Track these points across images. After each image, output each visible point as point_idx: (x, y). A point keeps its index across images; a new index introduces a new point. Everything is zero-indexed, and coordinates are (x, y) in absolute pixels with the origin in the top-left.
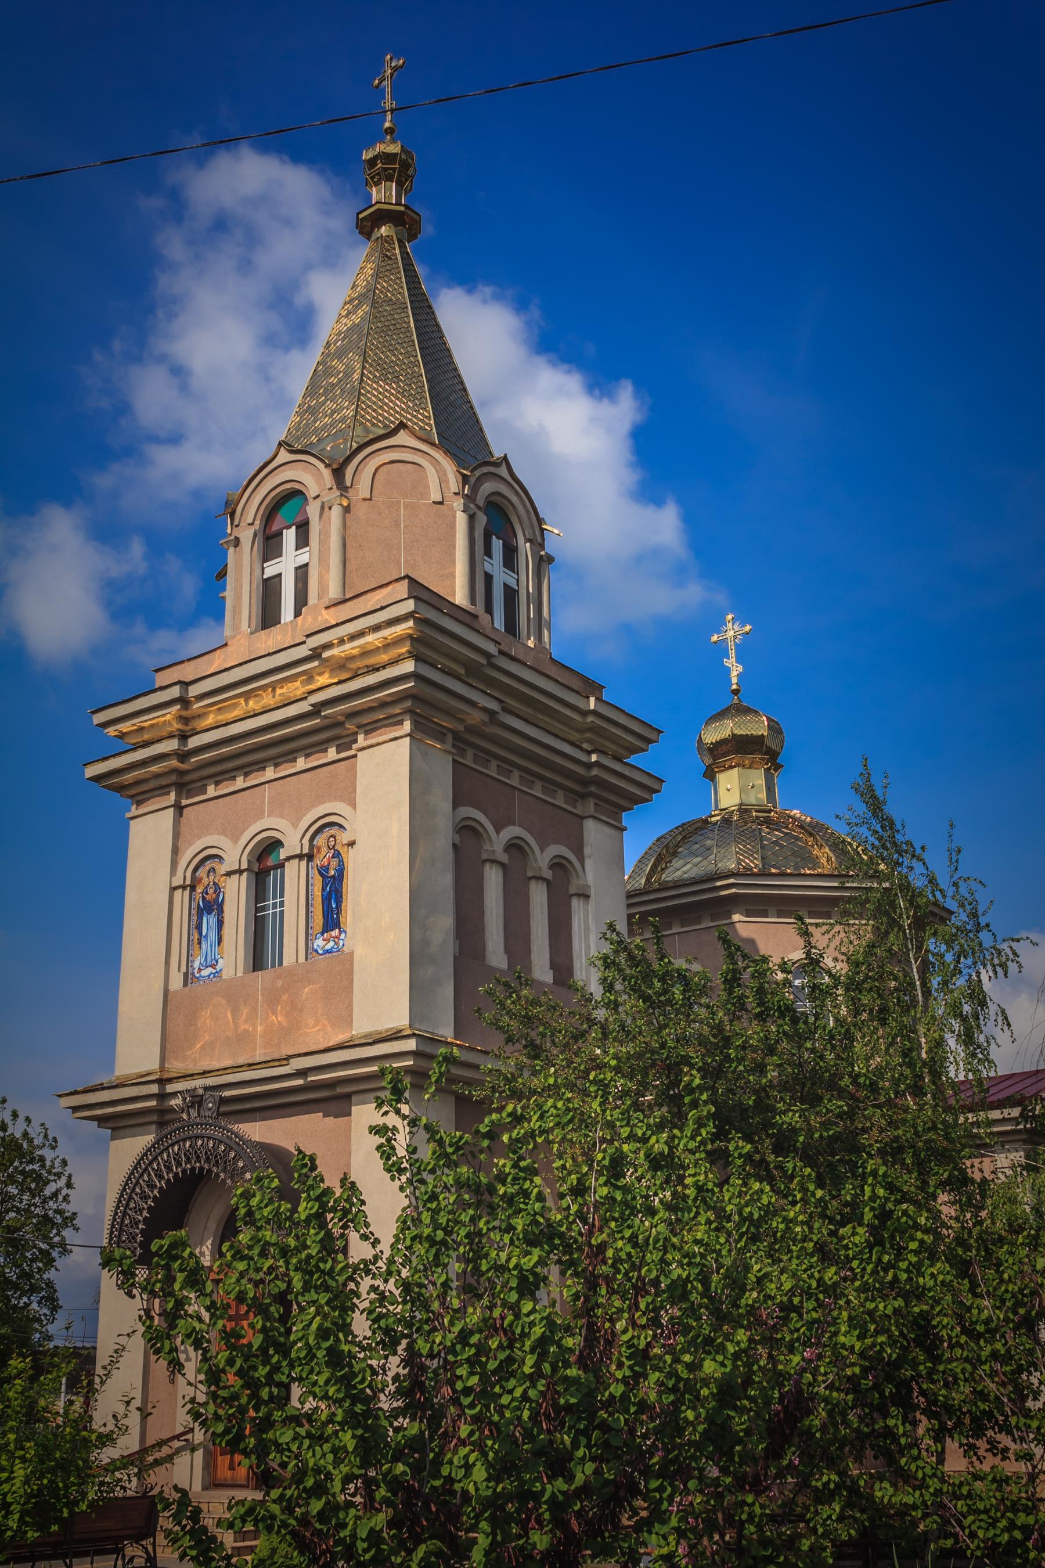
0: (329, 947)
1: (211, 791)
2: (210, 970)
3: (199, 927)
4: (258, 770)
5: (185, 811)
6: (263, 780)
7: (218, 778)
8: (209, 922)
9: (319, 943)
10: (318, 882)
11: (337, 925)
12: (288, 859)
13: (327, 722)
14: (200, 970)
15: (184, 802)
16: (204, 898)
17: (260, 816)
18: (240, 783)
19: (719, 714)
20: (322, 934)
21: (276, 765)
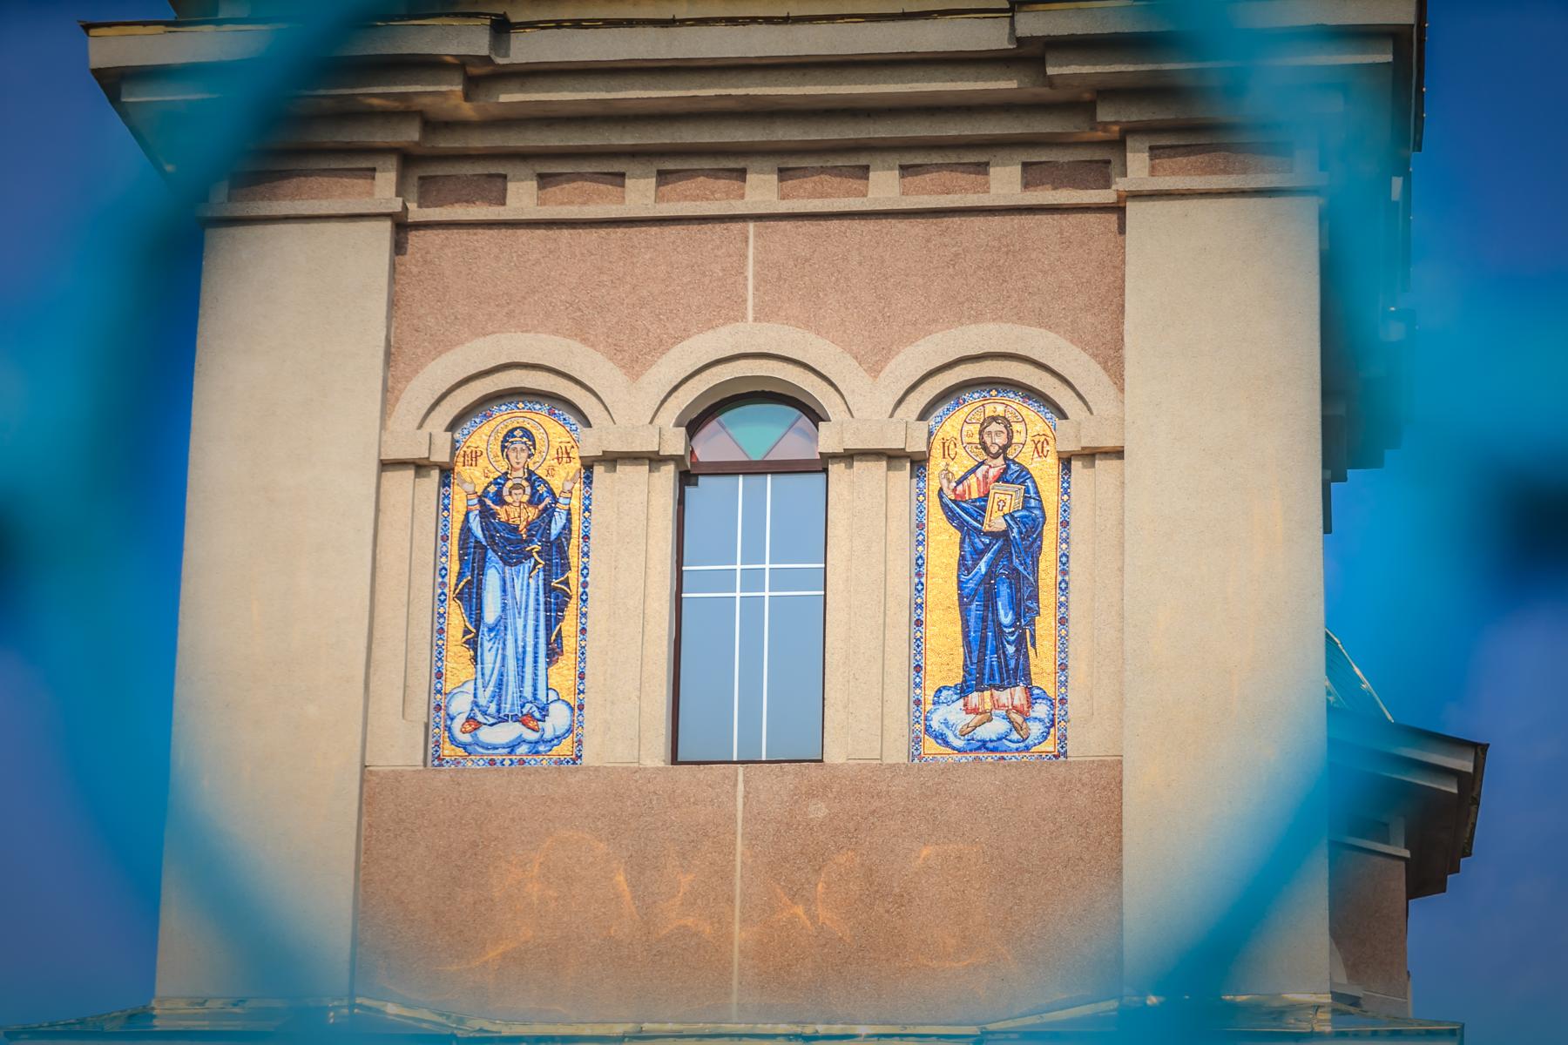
0: (989, 731)
1: (523, 197)
2: (508, 732)
3: (471, 597)
4: (715, 174)
5: (415, 239)
6: (739, 208)
7: (550, 167)
8: (510, 590)
9: (953, 714)
10: (944, 543)
11: (1015, 673)
12: (849, 456)
13: (1045, 92)
14: (473, 722)
15: (416, 213)
16: (486, 514)
17: (731, 310)
18: (640, 194)
19: (385, 401)
20: (963, 691)
21: (544, 180)
